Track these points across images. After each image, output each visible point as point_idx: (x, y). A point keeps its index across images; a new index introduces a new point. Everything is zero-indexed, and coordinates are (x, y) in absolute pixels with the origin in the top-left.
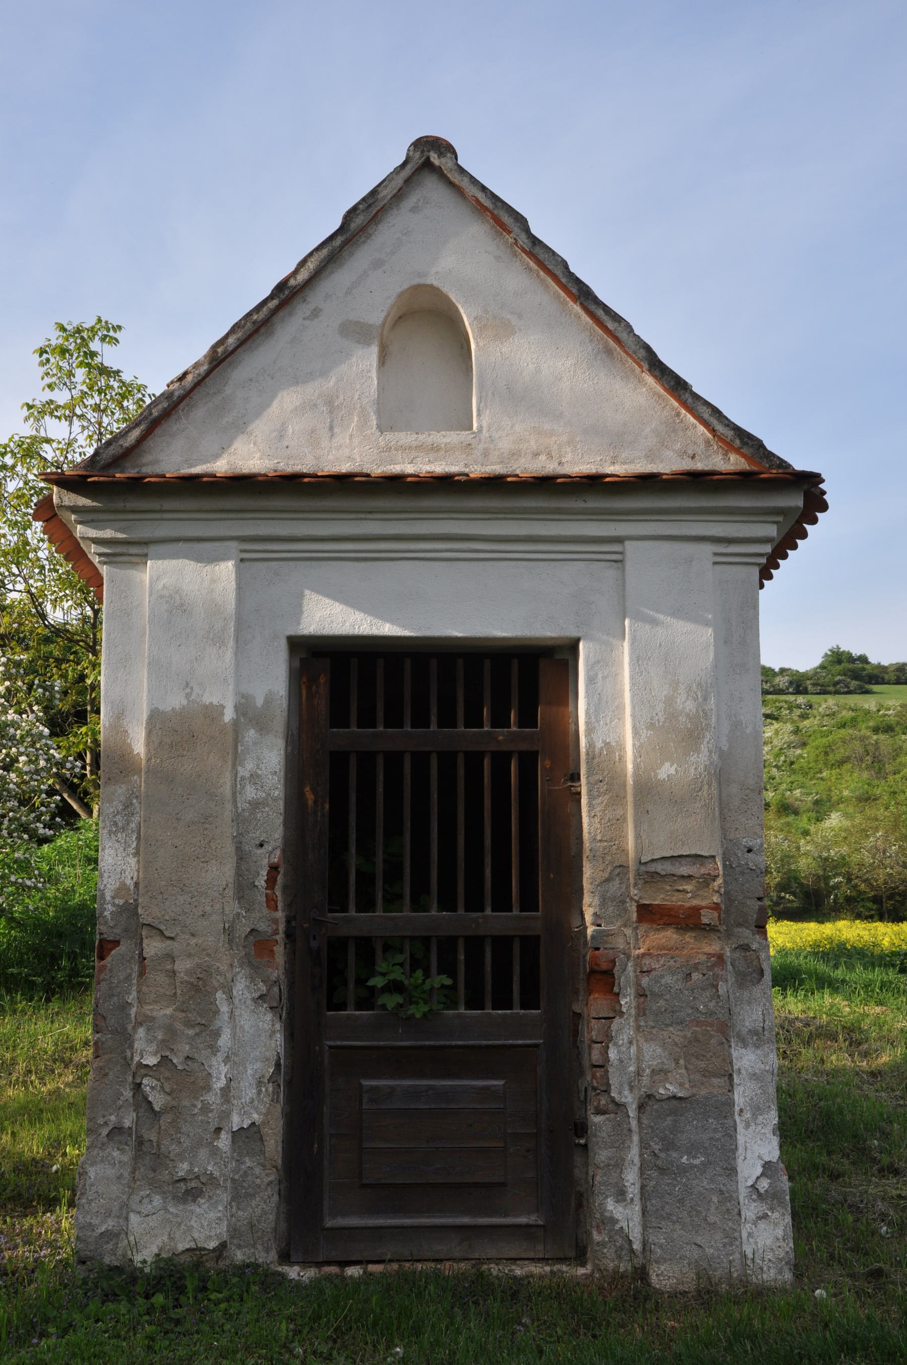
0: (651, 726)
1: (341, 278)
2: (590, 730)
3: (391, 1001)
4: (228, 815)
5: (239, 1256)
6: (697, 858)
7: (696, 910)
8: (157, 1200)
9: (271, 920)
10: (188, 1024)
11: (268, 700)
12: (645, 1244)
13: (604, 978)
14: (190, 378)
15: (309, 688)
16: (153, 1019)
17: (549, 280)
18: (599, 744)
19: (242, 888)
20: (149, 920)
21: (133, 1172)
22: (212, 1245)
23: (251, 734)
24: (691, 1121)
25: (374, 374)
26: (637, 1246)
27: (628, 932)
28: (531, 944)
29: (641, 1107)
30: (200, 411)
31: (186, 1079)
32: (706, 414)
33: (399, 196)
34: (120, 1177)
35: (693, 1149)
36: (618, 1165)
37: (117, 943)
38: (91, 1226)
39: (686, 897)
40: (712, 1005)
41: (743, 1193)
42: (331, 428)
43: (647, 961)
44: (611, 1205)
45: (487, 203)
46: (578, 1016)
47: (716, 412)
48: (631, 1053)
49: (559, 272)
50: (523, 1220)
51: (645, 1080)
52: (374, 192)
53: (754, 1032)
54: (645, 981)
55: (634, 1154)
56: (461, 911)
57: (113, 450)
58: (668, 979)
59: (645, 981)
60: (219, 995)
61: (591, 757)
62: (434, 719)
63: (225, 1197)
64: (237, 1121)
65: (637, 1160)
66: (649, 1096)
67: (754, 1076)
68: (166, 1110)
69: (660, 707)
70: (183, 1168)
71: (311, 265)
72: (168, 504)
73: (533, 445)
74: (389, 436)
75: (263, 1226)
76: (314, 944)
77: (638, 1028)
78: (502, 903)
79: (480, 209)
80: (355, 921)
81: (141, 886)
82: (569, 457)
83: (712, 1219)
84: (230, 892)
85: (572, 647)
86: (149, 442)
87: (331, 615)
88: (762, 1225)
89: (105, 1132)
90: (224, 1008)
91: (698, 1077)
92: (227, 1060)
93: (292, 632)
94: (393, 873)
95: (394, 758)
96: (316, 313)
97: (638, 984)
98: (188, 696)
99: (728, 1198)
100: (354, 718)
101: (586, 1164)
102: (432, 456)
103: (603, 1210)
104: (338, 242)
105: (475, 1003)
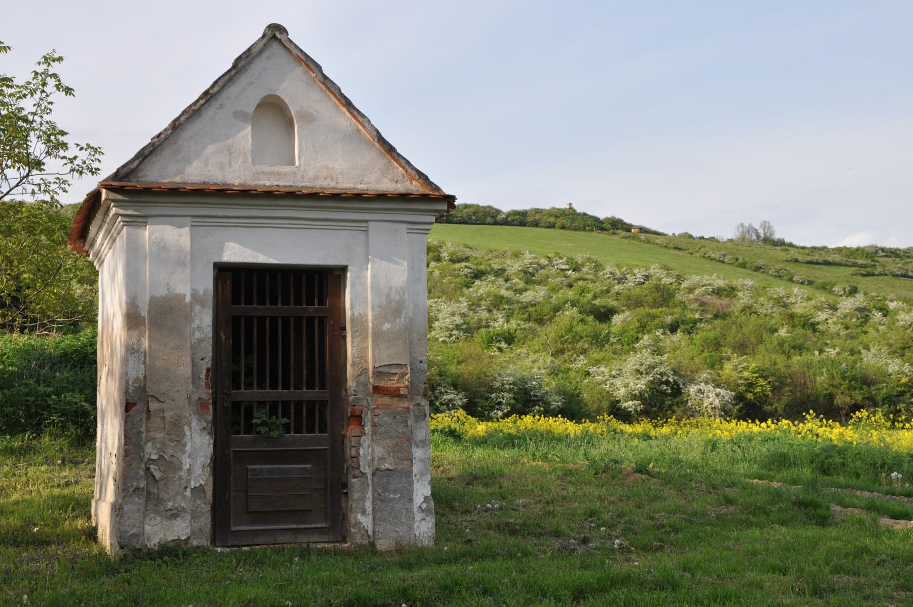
0: (380, 306)
1: (234, 90)
2: (352, 308)
3: (263, 430)
4: (188, 346)
5: (195, 543)
6: (399, 365)
7: (398, 388)
8: (158, 519)
9: (205, 393)
10: (171, 441)
11: (205, 292)
12: (374, 532)
13: (358, 418)
14: (162, 136)
15: (222, 286)
16: (155, 439)
17: (331, 96)
18: (356, 314)
19: (195, 379)
20: (152, 394)
21: (146, 507)
22: (184, 538)
23: (197, 308)
24: (394, 480)
25: (250, 137)
26: (370, 533)
27: (368, 398)
28: (323, 404)
29: (373, 474)
30: (167, 152)
31: (172, 465)
32: (403, 163)
33: (261, 51)
34: (139, 510)
35: (395, 491)
36: (363, 499)
37: (135, 404)
38: (126, 532)
39: (393, 383)
40: (405, 430)
41: (415, 509)
42: (230, 163)
43: (377, 411)
44: (359, 516)
45: (303, 58)
46: (344, 436)
47: (408, 162)
48: (369, 451)
49: (336, 93)
50: (319, 525)
51: (376, 462)
52: (249, 50)
53: (422, 441)
54: (376, 420)
55: (370, 495)
56: (292, 390)
57: (126, 170)
58: (386, 419)
59: (376, 420)
60: (186, 427)
61: (352, 319)
62: (280, 301)
63: (189, 517)
64: (193, 484)
65: (371, 497)
66: (377, 469)
67: (421, 460)
68: (161, 479)
69: (384, 298)
70: (170, 505)
71: (220, 84)
72: (159, 199)
73: (325, 174)
74: (257, 167)
75: (205, 530)
76: (226, 405)
77: (373, 440)
78: (310, 386)
79: (299, 60)
80: (246, 394)
81: (148, 378)
82: (341, 180)
83: (402, 520)
84: (190, 381)
85: (344, 269)
86: (142, 166)
87: (237, 252)
88: (423, 522)
89: (131, 490)
90: (188, 433)
91: (398, 461)
92: (189, 456)
93: (217, 260)
94: (249, 373)
95: (262, 319)
96: (222, 106)
97: (373, 421)
98: (168, 290)
99: (410, 511)
100: (243, 300)
101: (347, 502)
102: (278, 177)
103: (356, 518)
104: (233, 72)
105: (298, 430)
